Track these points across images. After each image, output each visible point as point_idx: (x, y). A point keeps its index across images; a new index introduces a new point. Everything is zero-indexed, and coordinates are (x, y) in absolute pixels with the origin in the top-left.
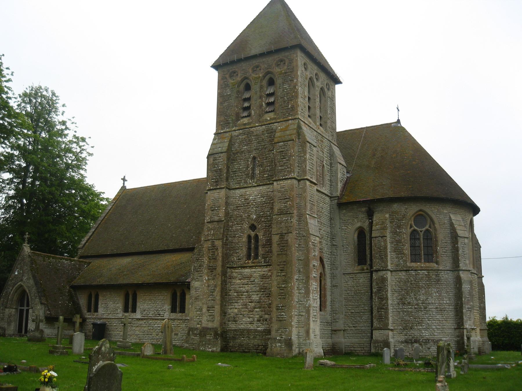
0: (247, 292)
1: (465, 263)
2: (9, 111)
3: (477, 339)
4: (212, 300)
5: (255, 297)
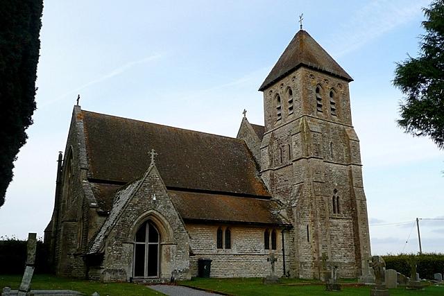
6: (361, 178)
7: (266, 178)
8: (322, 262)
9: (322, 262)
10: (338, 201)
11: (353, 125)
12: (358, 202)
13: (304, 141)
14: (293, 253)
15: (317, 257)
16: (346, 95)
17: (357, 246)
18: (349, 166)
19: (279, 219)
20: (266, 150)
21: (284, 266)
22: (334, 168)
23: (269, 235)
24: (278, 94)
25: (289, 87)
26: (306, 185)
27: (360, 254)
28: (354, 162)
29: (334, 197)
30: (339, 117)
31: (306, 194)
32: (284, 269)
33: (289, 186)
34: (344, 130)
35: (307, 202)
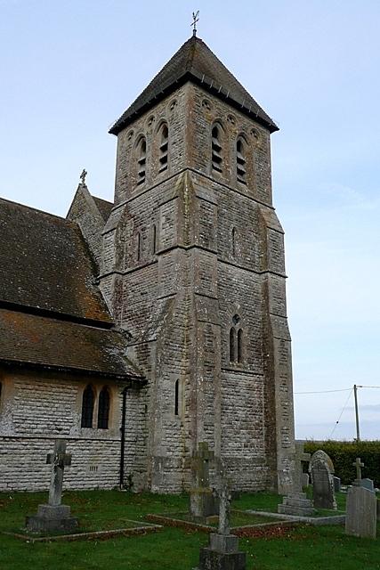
0: (233, 406)
1: (278, 383)
2: (196, 132)
3: (289, 478)
4: (210, 414)
5: (241, 414)
6: (283, 299)
7: (107, 288)
8: (201, 460)
9: (201, 460)
10: (239, 339)
11: (274, 206)
12: (277, 344)
13: (181, 214)
14: (143, 438)
15: (191, 448)
16: (265, 151)
17: (271, 427)
18: (263, 276)
19: (119, 366)
20: (112, 237)
21: (122, 465)
22: (237, 275)
23: (93, 398)
24: (142, 137)
25: (163, 122)
26: (179, 299)
27: (274, 443)
28: (273, 268)
29: (232, 331)
30: (250, 187)
31: (180, 316)
32: (122, 472)
33: (149, 304)
34: (258, 211)
35: (179, 333)
